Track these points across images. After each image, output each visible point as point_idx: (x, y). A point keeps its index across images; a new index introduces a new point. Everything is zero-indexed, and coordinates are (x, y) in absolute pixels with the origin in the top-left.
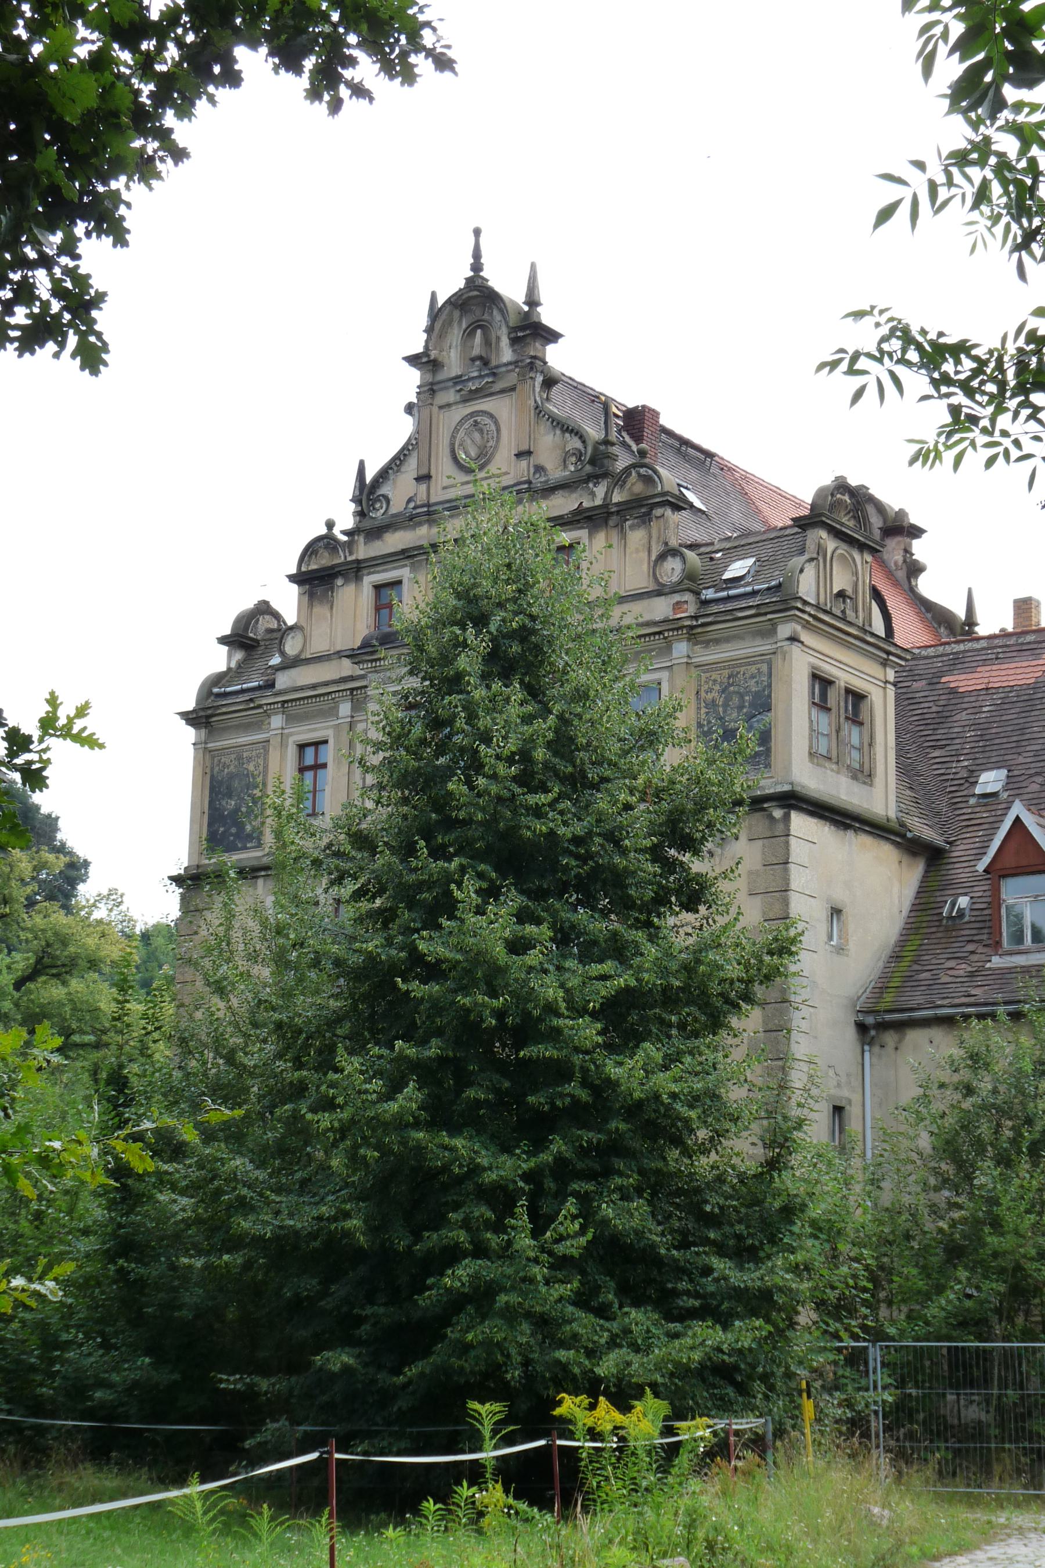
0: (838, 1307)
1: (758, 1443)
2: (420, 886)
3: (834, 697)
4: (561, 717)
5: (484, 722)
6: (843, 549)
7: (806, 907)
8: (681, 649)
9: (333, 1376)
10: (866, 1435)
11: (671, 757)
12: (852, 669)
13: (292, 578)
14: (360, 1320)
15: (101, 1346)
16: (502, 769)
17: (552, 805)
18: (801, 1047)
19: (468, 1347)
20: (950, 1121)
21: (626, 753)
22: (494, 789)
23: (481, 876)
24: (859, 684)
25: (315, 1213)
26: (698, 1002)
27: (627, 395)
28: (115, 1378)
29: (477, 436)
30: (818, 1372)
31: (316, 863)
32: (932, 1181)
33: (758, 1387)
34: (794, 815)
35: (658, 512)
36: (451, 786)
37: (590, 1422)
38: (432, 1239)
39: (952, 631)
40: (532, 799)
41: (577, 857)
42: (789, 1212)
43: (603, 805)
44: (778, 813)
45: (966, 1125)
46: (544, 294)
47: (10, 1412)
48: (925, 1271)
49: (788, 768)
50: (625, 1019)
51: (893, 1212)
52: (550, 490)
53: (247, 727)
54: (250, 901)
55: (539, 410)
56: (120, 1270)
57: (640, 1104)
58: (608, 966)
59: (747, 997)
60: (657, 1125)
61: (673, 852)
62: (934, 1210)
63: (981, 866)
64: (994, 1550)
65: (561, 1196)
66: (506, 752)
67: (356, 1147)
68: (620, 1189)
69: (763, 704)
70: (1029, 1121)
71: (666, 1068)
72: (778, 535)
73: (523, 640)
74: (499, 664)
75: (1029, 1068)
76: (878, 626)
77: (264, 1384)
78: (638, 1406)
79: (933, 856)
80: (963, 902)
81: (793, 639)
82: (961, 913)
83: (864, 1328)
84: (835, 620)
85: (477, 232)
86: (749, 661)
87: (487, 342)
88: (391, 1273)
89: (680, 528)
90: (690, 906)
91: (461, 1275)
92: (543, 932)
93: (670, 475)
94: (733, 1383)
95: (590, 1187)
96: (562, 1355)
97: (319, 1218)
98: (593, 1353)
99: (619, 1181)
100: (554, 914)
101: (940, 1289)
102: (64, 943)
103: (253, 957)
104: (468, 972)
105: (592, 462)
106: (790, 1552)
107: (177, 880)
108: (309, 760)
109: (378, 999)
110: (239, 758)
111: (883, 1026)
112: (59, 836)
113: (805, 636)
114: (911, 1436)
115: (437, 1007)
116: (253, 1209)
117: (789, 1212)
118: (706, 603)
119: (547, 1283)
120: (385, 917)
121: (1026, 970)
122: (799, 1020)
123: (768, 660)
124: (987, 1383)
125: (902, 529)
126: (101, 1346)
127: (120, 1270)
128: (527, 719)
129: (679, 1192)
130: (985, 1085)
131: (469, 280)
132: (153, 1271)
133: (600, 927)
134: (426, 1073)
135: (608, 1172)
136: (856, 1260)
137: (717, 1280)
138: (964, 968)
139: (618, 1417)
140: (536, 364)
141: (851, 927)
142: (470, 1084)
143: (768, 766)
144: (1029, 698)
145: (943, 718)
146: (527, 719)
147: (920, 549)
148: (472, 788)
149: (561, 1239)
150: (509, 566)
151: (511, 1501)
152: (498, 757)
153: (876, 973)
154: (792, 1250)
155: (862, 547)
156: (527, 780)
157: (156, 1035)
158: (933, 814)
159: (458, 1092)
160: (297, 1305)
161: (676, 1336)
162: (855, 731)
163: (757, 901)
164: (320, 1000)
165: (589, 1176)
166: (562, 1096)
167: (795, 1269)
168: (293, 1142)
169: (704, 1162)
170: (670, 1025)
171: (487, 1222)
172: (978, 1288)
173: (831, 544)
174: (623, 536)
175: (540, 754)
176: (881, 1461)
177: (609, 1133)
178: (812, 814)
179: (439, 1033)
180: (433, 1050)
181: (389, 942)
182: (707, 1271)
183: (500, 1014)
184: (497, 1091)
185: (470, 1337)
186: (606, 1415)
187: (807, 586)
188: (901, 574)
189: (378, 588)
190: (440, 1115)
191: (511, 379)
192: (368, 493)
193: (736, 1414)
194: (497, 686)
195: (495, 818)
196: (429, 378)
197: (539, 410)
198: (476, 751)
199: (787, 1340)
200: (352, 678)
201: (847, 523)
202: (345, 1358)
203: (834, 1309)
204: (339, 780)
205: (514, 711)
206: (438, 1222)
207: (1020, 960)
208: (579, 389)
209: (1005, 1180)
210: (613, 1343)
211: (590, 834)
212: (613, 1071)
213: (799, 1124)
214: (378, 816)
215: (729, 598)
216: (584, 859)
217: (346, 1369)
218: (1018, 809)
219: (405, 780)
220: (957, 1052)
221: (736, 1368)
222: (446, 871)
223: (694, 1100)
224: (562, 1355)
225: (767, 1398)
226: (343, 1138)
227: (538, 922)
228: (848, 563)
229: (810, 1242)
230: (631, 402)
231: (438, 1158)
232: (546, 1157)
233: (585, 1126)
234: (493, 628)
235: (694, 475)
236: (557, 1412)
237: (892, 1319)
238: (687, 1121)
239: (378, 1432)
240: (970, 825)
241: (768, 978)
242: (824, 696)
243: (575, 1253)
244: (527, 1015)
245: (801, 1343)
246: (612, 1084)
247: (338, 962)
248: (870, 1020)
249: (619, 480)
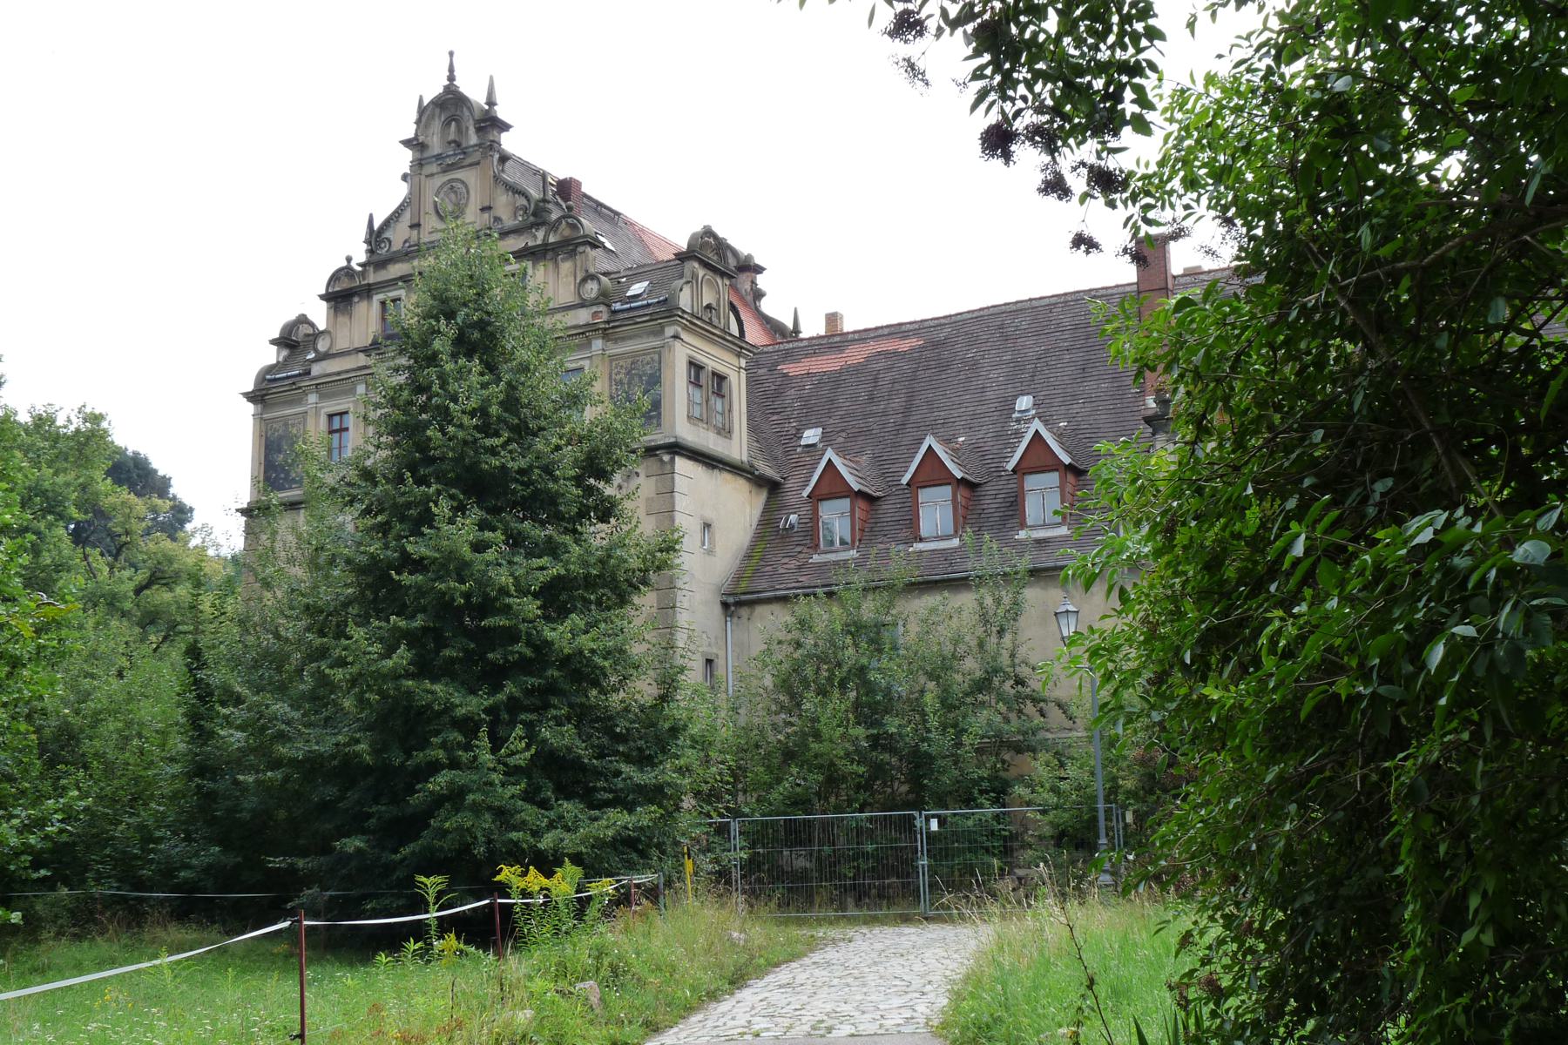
0: (709, 795)
1: (652, 893)
2: (408, 505)
3: (704, 378)
4: (509, 384)
5: (453, 386)
6: (710, 275)
7: (686, 521)
8: (598, 344)
9: (349, 857)
10: (728, 882)
11: (590, 413)
12: (717, 359)
13: (322, 297)
14: (369, 816)
15: (184, 840)
16: (466, 420)
17: (504, 446)
18: (683, 618)
19: (445, 833)
20: (786, 666)
21: (556, 410)
22: (461, 434)
23: (452, 497)
24: (721, 369)
25: (334, 740)
26: (610, 586)
27: (559, 172)
28: (194, 862)
29: (453, 196)
30: (697, 840)
31: (333, 490)
32: (774, 708)
33: (654, 852)
34: (677, 459)
35: (581, 249)
36: (429, 433)
37: (522, 885)
38: (419, 757)
39: (783, 335)
40: (489, 442)
41: (522, 483)
42: (675, 731)
43: (540, 446)
44: (666, 458)
45: (796, 669)
46: (499, 98)
47: (118, 889)
48: (769, 768)
49: (673, 426)
50: (558, 597)
51: (747, 729)
52: (504, 234)
54: (289, 522)
55: (496, 178)
56: (198, 786)
57: (569, 657)
58: (544, 561)
59: (645, 582)
60: (581, 671)
61: (592, 481)
62: (774, 727)
63: (805, 494)
64: (817, 957)
65: (512, 724)
66: (469, 408)
67: (363, 692)
68: (555, 717)
69: (655, 380)
70: (839, 665)
71: (586, 632)
72: (665, 265)
73: (482, 330)
74: (464, 345)
75: (839, 628)
76: (734, 330)
77: (301, 863)
78: (559, 872)
79: (773, 487)
80: (793, 518)
81: (676, 337)
82: (792, 526)
83: (727, 809)
84: (704, 324)
85: (451, 54)
86: (645, 352)
87: (459, 130)
88: (391, 781)
89: (598, 261)
90: (604, 519)
91: (440, 781)
92: (498, 536)
93: (589, 225)
94: (637, 851)
95: (533, 717)
96: (514, 835)
97: (337, 745)
98: (537, 834)
99: (554, 712)
100: (506, 525)
101: (779, 781)
102: (170, 561)
103: (291, 561)
104: (443, 565)
105: (534, 214)
106: (674, 969)
107: (243, 512)
108: (336, 426)
109: (378, 587)
110: (286, 425)
111: (739, 604)
112: (172, 491)
114: (759, 881)
115: (421, 591)
116: (290, 739)
117: (675, 731)
118: (615, 312)
119: (503, 785)
120: (384, 529)
121: (836, 563)
122: (683, 600)
123: (659, 351)
124: (811, 841)
125: (749, 268)
126: (184, 840)
127: (198, 786)
128: (484, 386)
129: (598, 719)
130: (809, 641)
131: (446, 88)
132: (222, 785)
133: (539, 533)
134: (412, 638)
135: (547, 706)
136: (722, 763)
137: (624, 780)
138: (794, 563)
139: (545, 882)
140: (494, 146)
141: (717, 536)
142: (446, 646)
143: (659, 425)
144: (835, 380)
145: (778, 393)
146: (484, 386)
147: (762, 281)
148: (444, 434)
149: (513, 753)
150: (471, 277)
151: (461, 946)
153: (735, 568)
154: (677, 757)
155: (723, 274)
156: (487, 429)
157: (222, 619)
158: (773, 460)
159: (437, 652)
160: (325, 807)
161: (596, 819)
162: (719, 402)
163: (653, 518)
164: (340, 586)
165: (535, 710)
166: (512, 653)
167: (680, 771)
168: (321, 691)
170: (590, 602)
171: (459, 743)
172: (805, 779)
173: (701, 272)
174: (557, 266)
175: (494, 410)
176: (739, 899)
177: (547, 678)
178: (690, 458)
179: (424, 610)
180: (418, 622)
181: (386, 547)
182: (618, 773)
183: (467, 596)
184: (466, 651)
185: (447, 825)
186: (535, 879)
187: (685, 300)
188: (749, 298)
190: (424, 668)
191: (476, 157)
192: (375, 237)
193: (638, 872)
194: (462, 361)
195: (462, 456)
196: (418, 155)
197: (496, 178)
198: (447, 408)
199: (675, 819)
200: (366, 367)
201: (713, 258)
202: (358, 843)
203: (707, 797)
204: (351, 434)
205: (474, 379)
206: (424, 744)
207: (832, 557)
208: (525, 166)
209: (823, 705)
210: (551, 826)
211: (531, 467)
212: (549, 634)
213: (682, 670)
214: (379, 458)
215: (631, 309)
216: (526, 485)
217: (358, 850)
218: (830, 454)
219: (395, 430)
220: (790, 619)
221: (638, 840)
222: (426, 494)
224: (514, 835)
225: (660, 859)
226: (353, 686)
227: (494, 530)
229: (689, 752)
230: (562, 174)
231: (422, 699)
232: (501, 697)
233: (530, 674)
234: (459, 320)
235: (607, 226)
236: (498, 878)
237: (747, 803)
238: (602, 668)
239: (382, 895)
240: (798, 465)
241: (659, 568)
242: (697, 377)
243: (522, 763)
244: (486, 596)
245: (684, 821)
246: (549, 644)
247: (348, 561)
248: (731, 600)
249: (554, 227)
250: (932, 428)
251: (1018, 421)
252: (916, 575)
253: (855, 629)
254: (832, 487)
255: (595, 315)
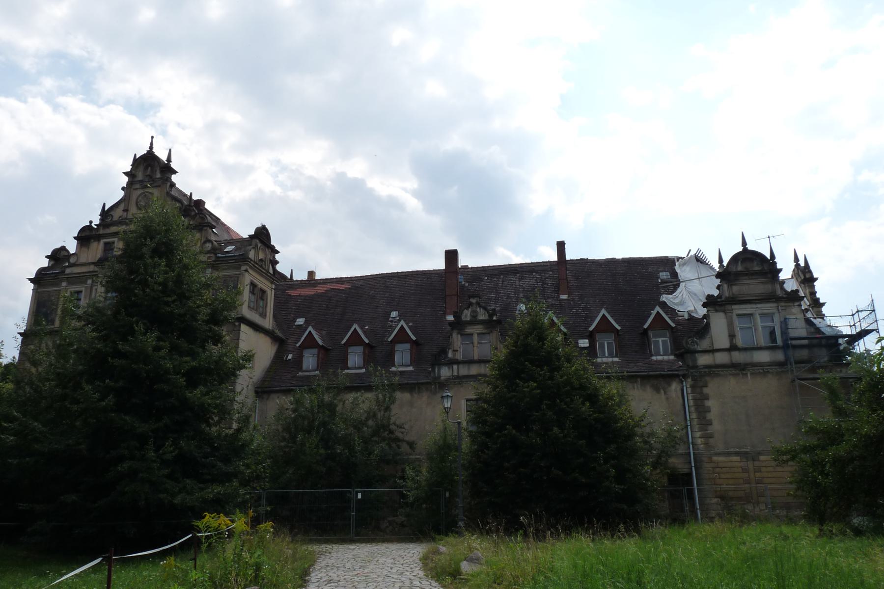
12: (263, 283)
16: (156, 287)
43: (191, 304)
44: (237, 324)
50: (193, 378)
53: (53, 285)
55: (168, 194)
58: (188, 359)
60: (202, 414)
81: (246, 271)
85: (152, 137)
87: (152, 171)
91: (125, 465)
96: (161, 496)
111: (264, 392)
113: (250, 271)
128: (166, 273)
144: (311, 299)
152: (155, 283)
169: (214, 429)
173: (259, 245)
180: (121, 384)
187: (252, 255)
189: (106, 244)
218: (310, 329)
223: (217, 407)
224: (161, 496)
228: (264, 251)
242: (253, 290)
250: (355, 321)
251: (392, 321)
252: (348, 384)
253: (322, 405)
254: (310, 343)
255: (209, 258)
